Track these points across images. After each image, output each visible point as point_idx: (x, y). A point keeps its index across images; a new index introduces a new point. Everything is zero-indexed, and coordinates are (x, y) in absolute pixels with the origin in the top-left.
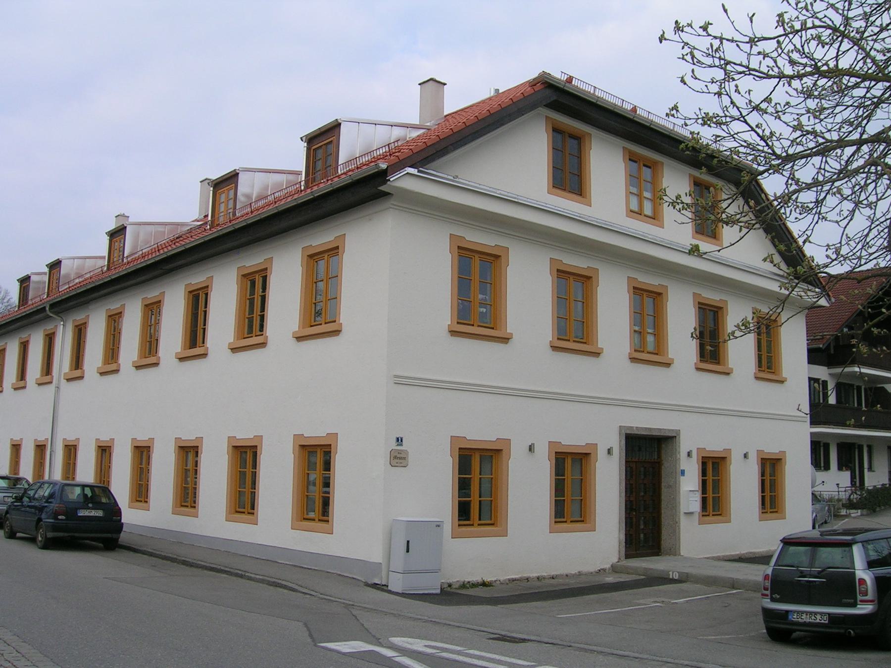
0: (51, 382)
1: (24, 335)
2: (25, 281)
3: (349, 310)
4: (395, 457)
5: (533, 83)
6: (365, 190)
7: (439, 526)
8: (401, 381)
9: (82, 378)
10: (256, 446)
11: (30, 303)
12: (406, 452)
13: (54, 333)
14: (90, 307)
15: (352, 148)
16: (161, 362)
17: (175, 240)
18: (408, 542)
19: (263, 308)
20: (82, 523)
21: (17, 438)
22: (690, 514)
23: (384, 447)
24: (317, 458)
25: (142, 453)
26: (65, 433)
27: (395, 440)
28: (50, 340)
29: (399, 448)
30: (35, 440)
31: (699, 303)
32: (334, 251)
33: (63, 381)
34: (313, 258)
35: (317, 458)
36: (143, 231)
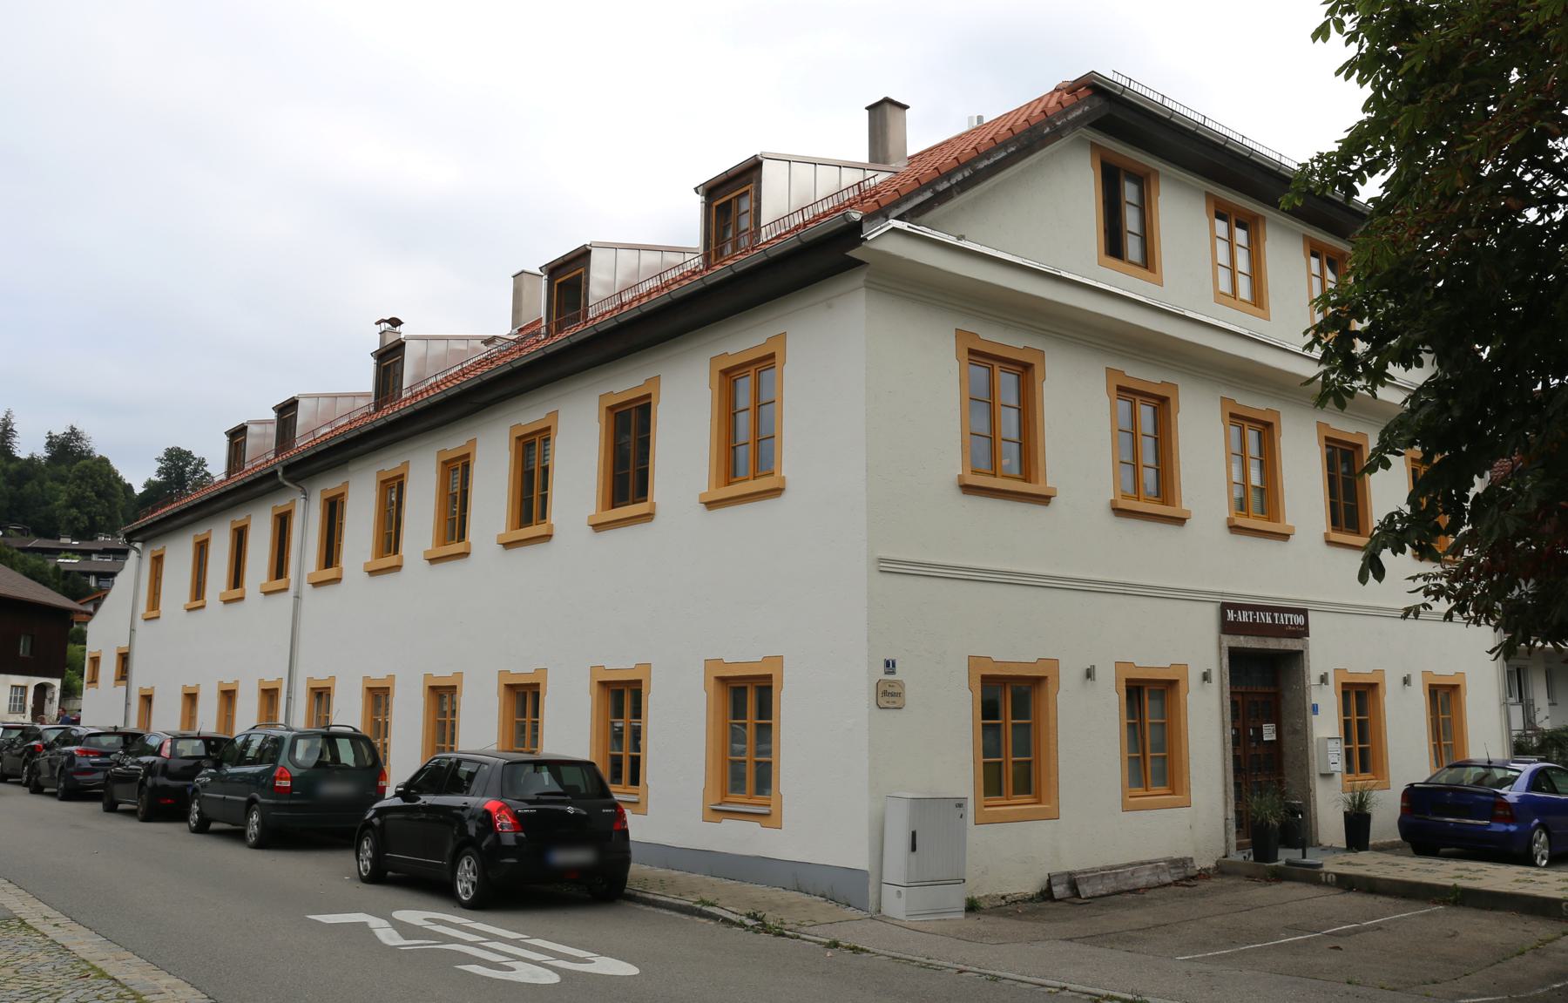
0: (286, 590)
1: (239, 517)
2: (237, 436)
3: (792, 459)
4: (885, 693)
5: (1073, 88)
6: (825, 255)
7: (960, 805)
8: (889, 567)
9: (337, 580)
10: (769, 677)
11: (247, 467)
12: (901, 684)
13: (290, 512)
14: (352, 468)
15: (605, 284)
16: (555, 532)
17: (463, 372)
18: (914, 834)
19: (545, 486)
20: (550, 842)
21: (191, 684)
22: (1327, 776)
23: (862, 679)
24: (747, 699)
25: (441, 697)
26: (312, 670)
27: (883, 664)
28: (283, 524)
29: (890, 677)
30: (261, 681)
31: (1327, 439)
32: (767, 361)
33: (307, 587)
34: (729, 377)
35: (747, 699)
36: (628, 259)
